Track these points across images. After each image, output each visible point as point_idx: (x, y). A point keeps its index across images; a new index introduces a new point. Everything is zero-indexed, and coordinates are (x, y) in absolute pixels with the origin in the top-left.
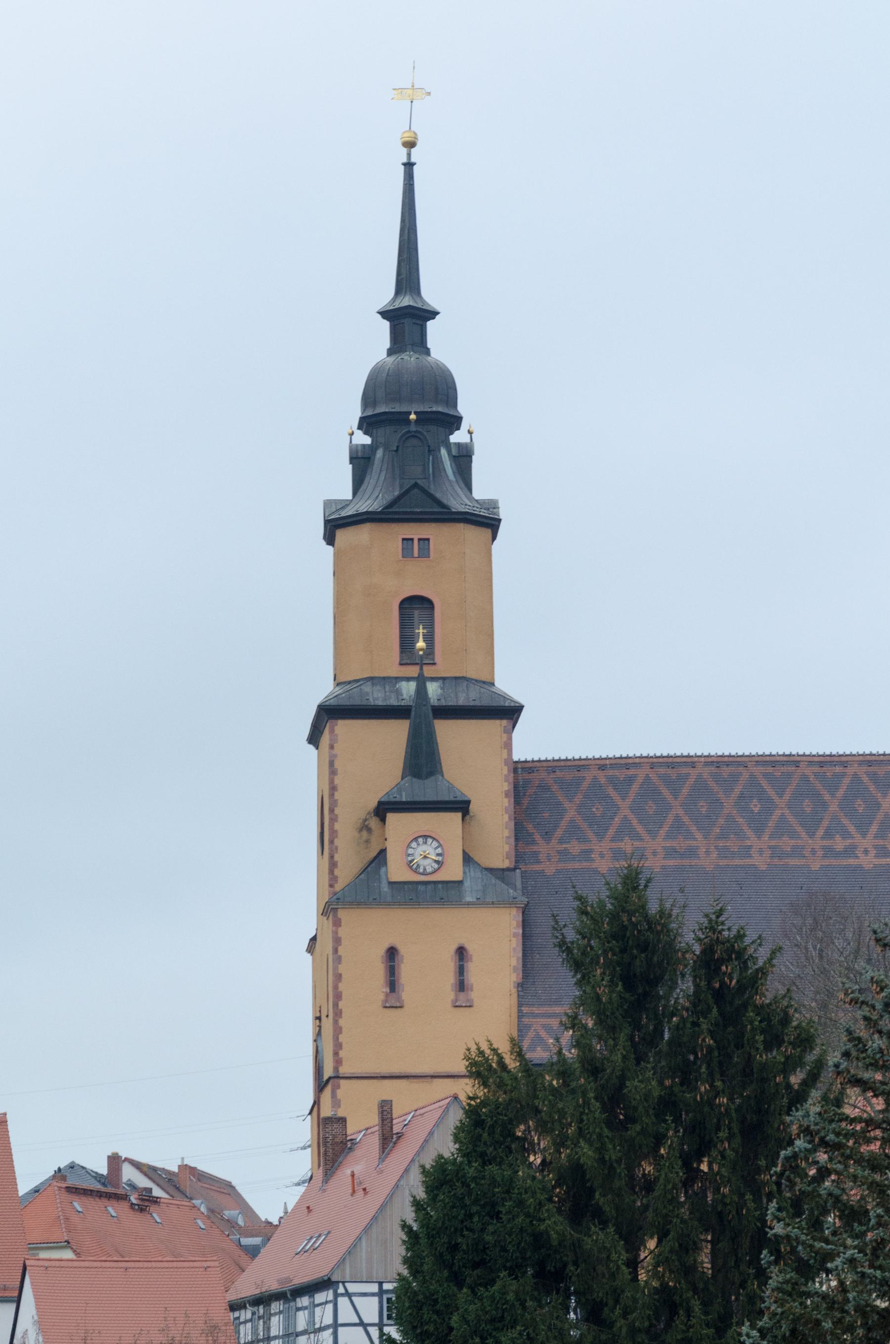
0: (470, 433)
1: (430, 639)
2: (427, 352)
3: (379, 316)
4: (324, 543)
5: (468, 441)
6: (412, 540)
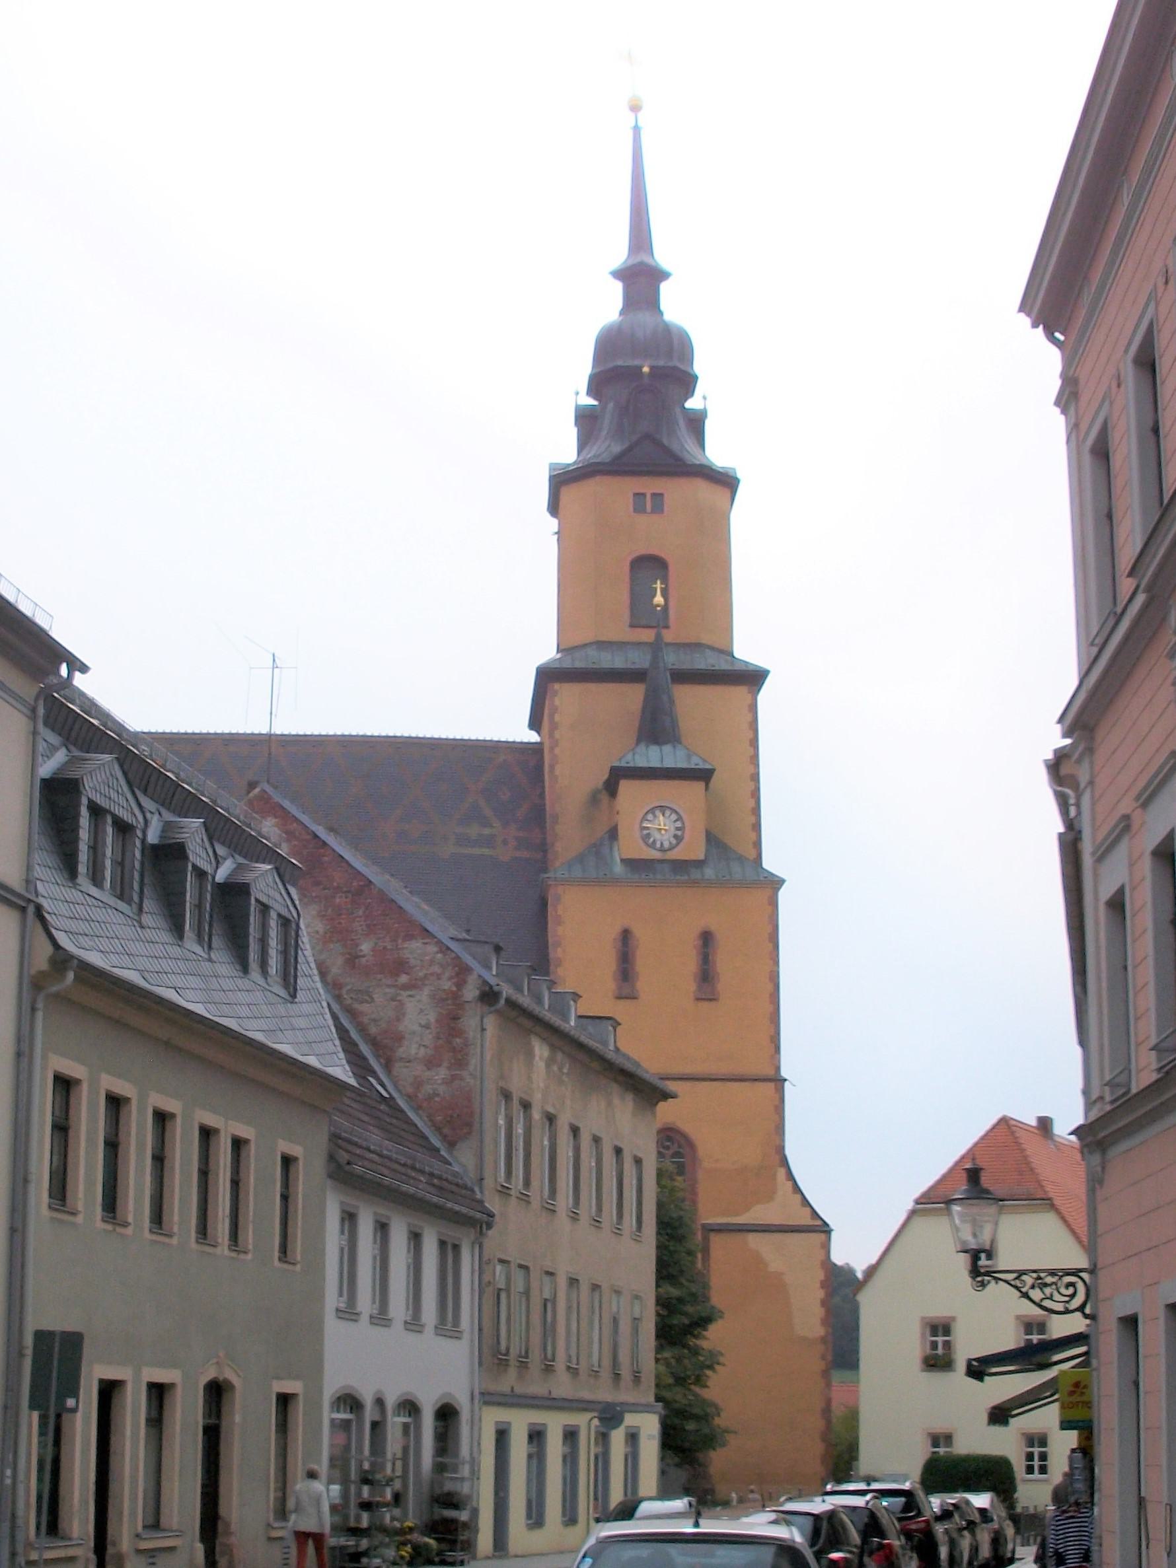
0: (705, 398)
1: (665, 594)
2: (661, 313)
4: (548, 515)
5: (702, 407)
6: (644, 495)
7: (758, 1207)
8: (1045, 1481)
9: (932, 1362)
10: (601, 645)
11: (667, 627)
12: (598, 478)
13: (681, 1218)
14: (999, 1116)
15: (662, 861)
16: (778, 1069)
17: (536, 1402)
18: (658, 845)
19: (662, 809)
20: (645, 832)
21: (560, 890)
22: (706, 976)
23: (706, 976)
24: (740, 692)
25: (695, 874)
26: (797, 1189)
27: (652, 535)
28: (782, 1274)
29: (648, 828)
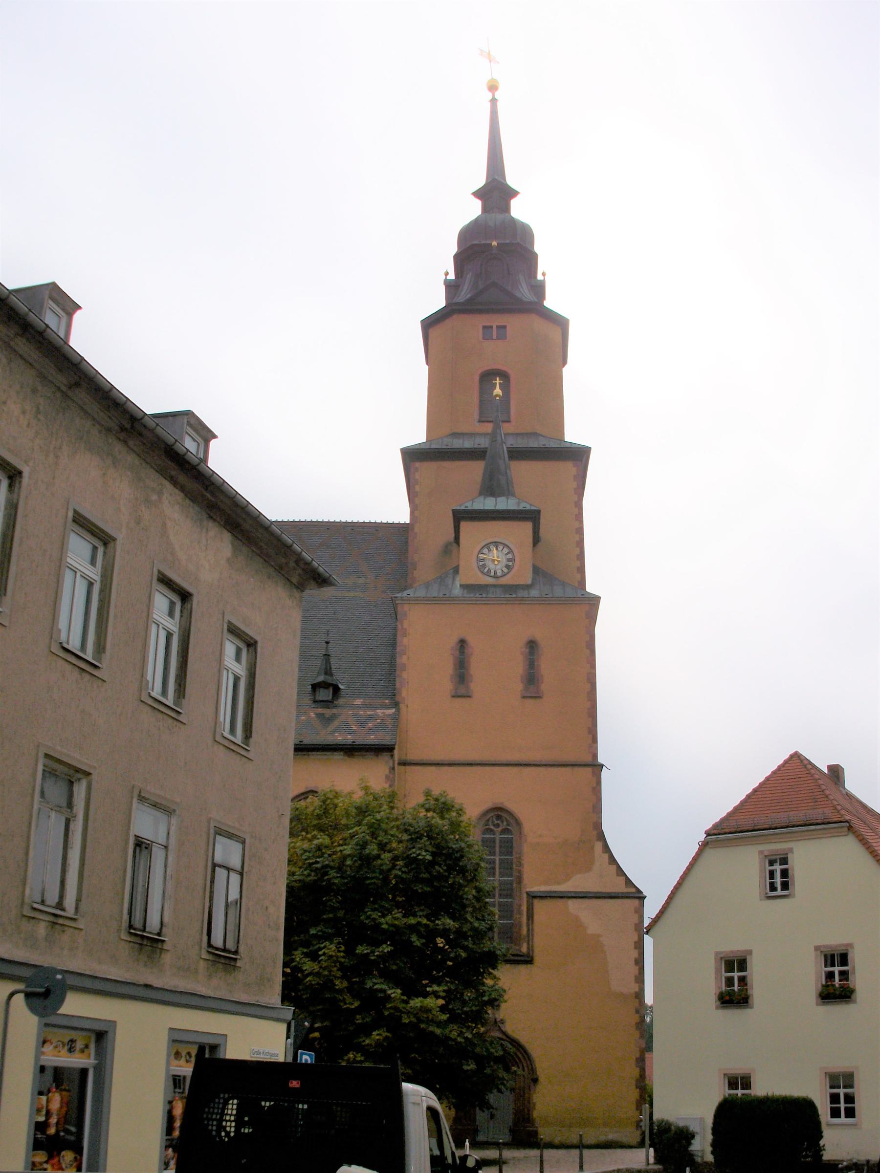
3: (473, 197)
6: (491, 327)
8: (855, 1125)
9: (727, 998)
10: (455, 435)
11: (509, 421)
12: (455, 316)
13: (461, 850)
14: (792, 752)
15: (494, 586)
16: (595, 756)
17: (98, 985)
18: (492, 574)
19: (496, 544)
20: (481, 563)
21: (406, 607)
22: (532, 679)
24: (568, 468)
25: (523, 593)
26: (612, 860)
27: (495, 354)
28: (599, 936)
29: (483, 560)
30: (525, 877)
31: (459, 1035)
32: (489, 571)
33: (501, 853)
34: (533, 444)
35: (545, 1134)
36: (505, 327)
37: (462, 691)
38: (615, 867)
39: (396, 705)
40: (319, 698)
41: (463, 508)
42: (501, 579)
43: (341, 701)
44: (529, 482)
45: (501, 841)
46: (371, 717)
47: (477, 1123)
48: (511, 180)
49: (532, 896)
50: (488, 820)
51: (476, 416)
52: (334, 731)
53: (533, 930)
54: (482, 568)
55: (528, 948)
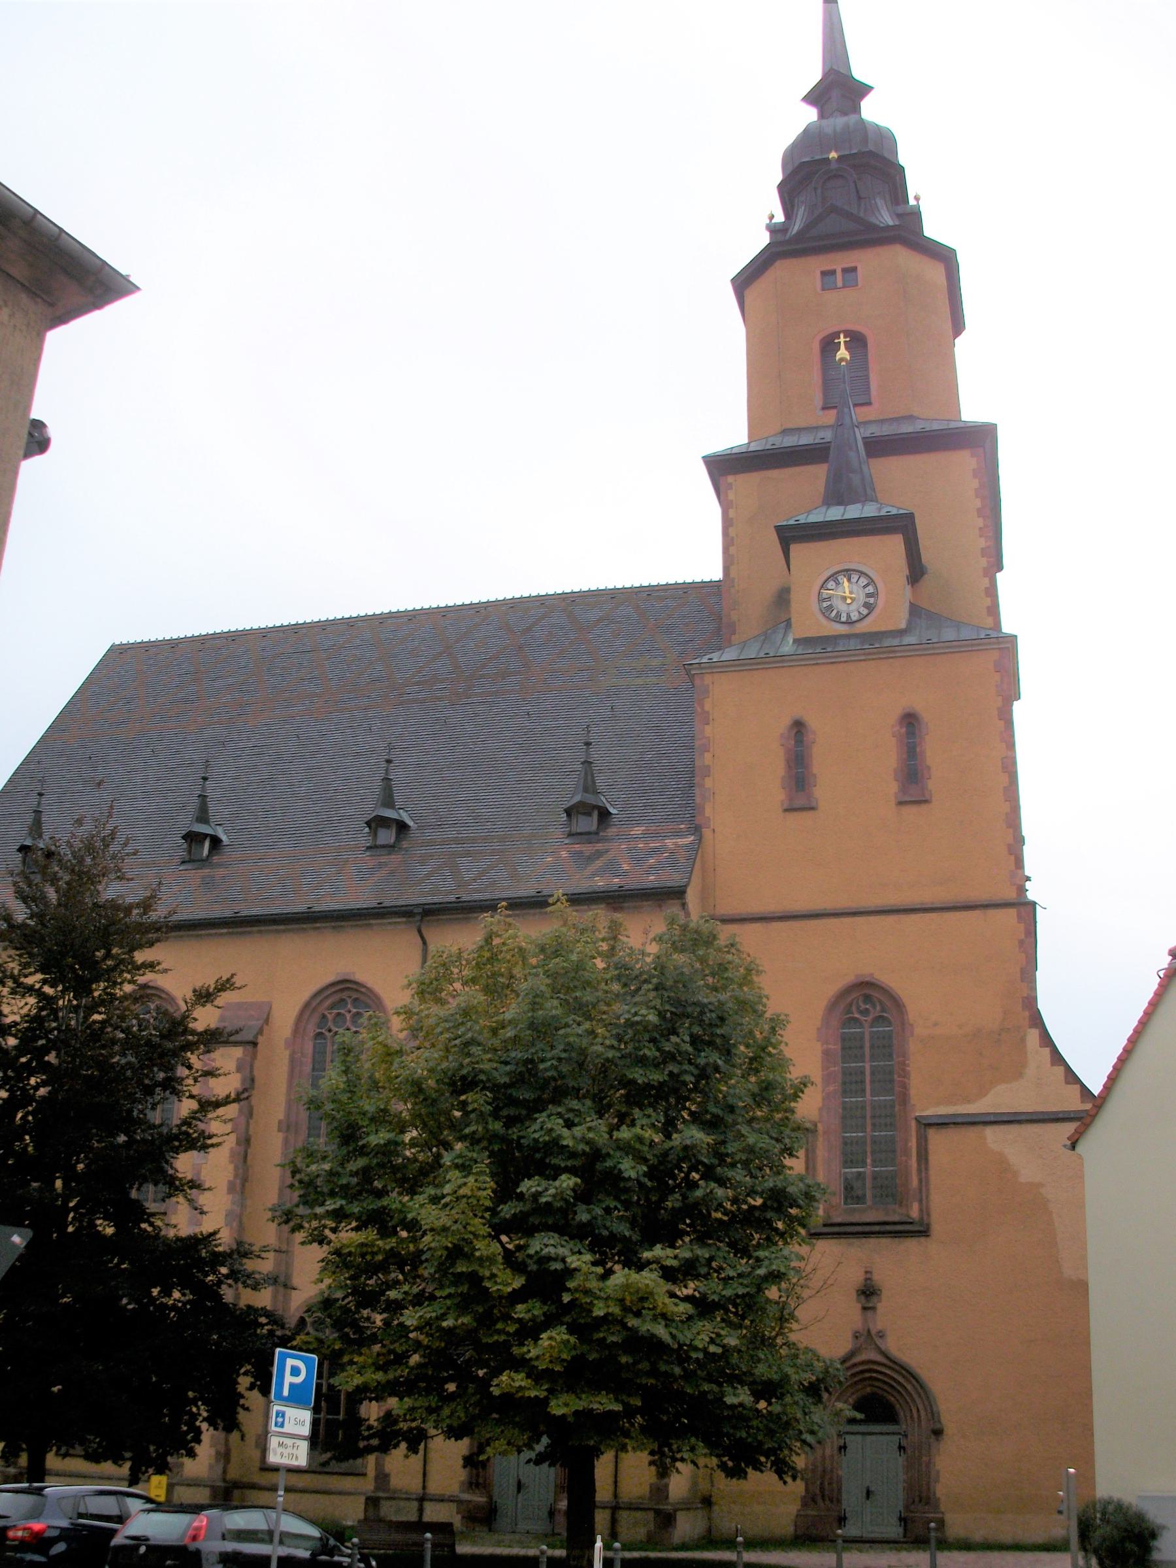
6: (833, 272)
7: (1001, 1088)
10: (785, 432)
12: (778, 264)
15: (848, 637)
16: (1019, 881)
19: (848, 573)
20: (825, 604)
21: (708, 679)
22: (913, 781)
23: (913, 781)
26: (1057, 1058)
27: (843, 309)
30: (913, 1092)
31: (712, 1341)
32: (839, 615)
33: (873, 1057)
34: (906, 428)
35: (957, 1525)
36: (854, 269)
37: (799, 803)
38: (1062, 1068)
39: (697, 830)
40: (576, 829)
41: (792, 522)
42: (858, 625)
43: (611, 831)
44: (897, 483)
45: (872, 1038)
46: (656, 851)
47: (844, 1505)
48: (860, 71)
49: (927, 1124)
50: (851, 1005)
51: (818, 400)
52: (594, 875)
53: (927, 1178)
54: (827, 612)
55: (921, 1210)
